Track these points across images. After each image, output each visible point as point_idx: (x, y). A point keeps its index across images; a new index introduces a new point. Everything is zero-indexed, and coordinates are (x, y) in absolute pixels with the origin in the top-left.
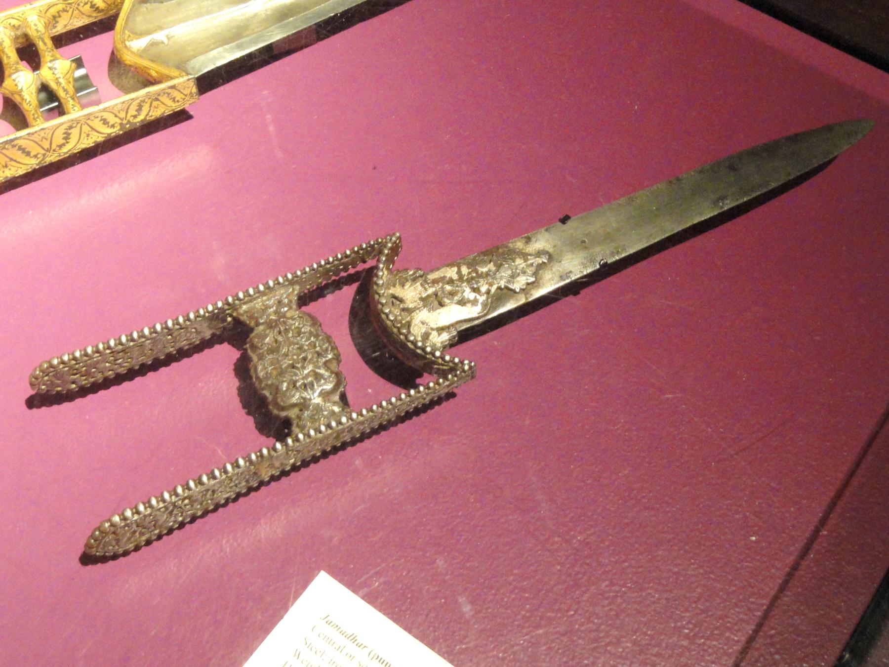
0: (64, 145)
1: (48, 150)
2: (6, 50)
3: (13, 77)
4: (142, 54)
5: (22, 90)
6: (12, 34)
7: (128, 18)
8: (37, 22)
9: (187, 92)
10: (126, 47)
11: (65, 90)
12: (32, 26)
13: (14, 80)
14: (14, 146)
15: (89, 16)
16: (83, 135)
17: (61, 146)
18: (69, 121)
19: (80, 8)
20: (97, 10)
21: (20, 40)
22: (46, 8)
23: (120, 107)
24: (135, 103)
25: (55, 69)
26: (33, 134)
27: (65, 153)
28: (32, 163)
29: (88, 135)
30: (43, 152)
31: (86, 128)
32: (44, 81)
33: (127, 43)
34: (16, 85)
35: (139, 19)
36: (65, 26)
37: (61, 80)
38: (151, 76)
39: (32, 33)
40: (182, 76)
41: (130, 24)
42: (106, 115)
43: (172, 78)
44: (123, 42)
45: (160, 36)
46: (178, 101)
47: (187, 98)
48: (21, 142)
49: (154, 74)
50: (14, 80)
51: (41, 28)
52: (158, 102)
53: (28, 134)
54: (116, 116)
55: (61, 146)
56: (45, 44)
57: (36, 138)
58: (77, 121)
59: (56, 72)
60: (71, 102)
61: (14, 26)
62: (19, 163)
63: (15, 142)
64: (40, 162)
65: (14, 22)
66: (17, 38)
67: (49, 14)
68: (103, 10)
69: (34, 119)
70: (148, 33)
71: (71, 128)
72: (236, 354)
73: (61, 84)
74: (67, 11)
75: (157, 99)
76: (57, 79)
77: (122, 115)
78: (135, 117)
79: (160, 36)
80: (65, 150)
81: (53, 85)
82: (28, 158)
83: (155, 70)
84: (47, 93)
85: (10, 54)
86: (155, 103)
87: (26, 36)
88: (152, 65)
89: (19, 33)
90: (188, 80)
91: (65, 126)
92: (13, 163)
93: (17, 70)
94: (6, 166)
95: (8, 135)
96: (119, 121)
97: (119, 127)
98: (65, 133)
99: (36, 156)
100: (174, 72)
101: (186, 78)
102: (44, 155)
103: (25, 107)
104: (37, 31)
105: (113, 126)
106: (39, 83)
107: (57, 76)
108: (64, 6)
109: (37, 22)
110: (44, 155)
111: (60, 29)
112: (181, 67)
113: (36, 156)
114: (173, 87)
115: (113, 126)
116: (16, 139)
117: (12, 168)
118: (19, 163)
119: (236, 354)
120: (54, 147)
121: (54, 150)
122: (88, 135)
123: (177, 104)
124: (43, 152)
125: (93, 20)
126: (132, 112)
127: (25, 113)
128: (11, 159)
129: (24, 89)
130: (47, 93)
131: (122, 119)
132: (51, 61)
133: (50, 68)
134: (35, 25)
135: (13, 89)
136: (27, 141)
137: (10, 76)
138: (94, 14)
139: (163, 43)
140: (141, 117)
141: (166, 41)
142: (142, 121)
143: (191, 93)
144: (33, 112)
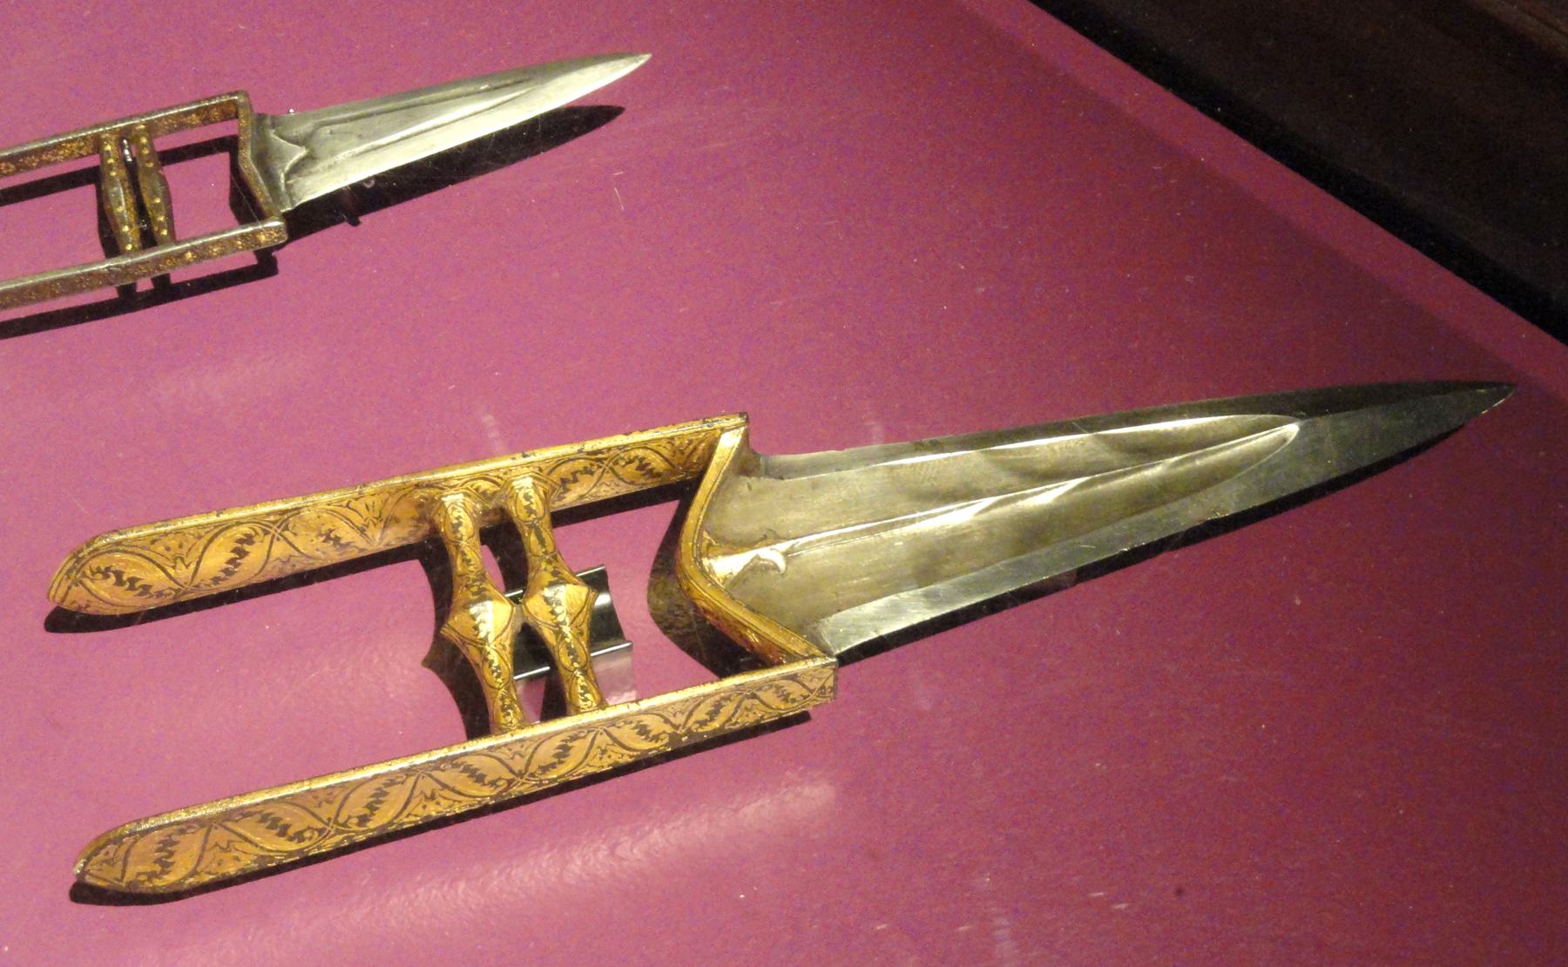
0: (553, 766)
1: (521, 775)
2: (463, 543)
3: (473, 610)
4: (737, 583)
5: (485, 640)
6: (478, 506)
7: (711, 504)
8: (532, 493)
9: (815, 685)
10: (703, 571)
11: (571, 652)
12: (521, 495)
13: (473, 617)
14: (457, 766)
15: (632, 483)
16: (595, 751)
17: (545, 769)
18: (573, 728)
19: (616, 468)
20: (652, 474)
21: (492, 517)
22: (552, 464)
23: (678, 708)
24: (710, 701)
25: (559, 603)
26: (499, 747)
27: (552, 781)
28: (486, 794)
29: (604, 752)
30: (511, 776)
31: (603, 740)
32: (530, 621)
33: (706, 562)
34: (476, 628)
35: (734, 507)
36: (582, 497)
37: (566, 629)
38: (747, 641)
39: (518, 512)
40: (813, 657)
41: (714, 520)
42: (647, 720)
43: (793, 658)
44: (698, 560)
45: (772, 554)
46: (794, 701)
47: (812, 696)
48: (473, 762)
49: (753, 638)
50: (473, 617)
51: (537, 505)
52: (756, 702)
53: (490, 748)
54: (667, 721)
55: (545, 769)
56: (542, 542)
57: (505, 755)
58: (589, 728)
59: (558, 610)
60: (581, 680)
61: (484, 493)
62: (460, 793)
63: (459, 761)
64: (499, 794)
65: (484, 485)
66: (486, 512)
67: (555, 477)
68: (659, 475)
69: (503, 709)
70: (749, 544)
71: (574, 738)
72: (445, 631)
73: (564, 637)
74: (592, 473)
75: (754, 696)
76: (558, 625)
77: (680, 719)
78: (703, 723)
79: (772, 554)
80: (553, 775)
81: (548, 635)
82: (478, 785)
83: (758, 630)
84: (530, 645)
85: (470, 555)
86: (748, 703)
87: (502, 511)
88: (752, 620)
89: (490, 506)
90: (824, 666)
91: (565, 736)
92: (446, 793)
93: (482, 597)
94: (433, 797)
95: (450, 745)
96: (669, 729)
97: (666, 741)
98: (560, 747)
99: (493, 783)
100: (797, 645)
101: (819, 662)
102: (510, 782)
103: (489, 676)
104: (530, 511)
105: (656, 738)
106: (519, 624)
107: (560, 619)
108: (587, 463)
109: (532, 493)
110: (510, 782)
111: (571, 498)
112: (805, 626)
113: (493, 783)
114: (793, 677)
115: (656, 738)
116: (466, 754)
117: (443, 802)
118: (460, 793)
119: (445, 631)
120: (532, 769)
121: (532, 775)
122: (604, 752)
123: (790, 705)
124: (511, 776)
125: (633, 489)
126: (701, 714)
127: (486, 690)
128: (445, 786)
129: (491, 638)
130: (530, 645)
131: (676, 727)
132: (551, 584)
133: (547, 600)
134: (527, 497)
135: (469, 634)
136: (487, 759)
137: (466, 607)
138: (642, 481)
139: (776, 568)
140: (716, 724)
141: (782, 565)
142: (714, 731)
143: (823, 687)
144: (502, 692)
